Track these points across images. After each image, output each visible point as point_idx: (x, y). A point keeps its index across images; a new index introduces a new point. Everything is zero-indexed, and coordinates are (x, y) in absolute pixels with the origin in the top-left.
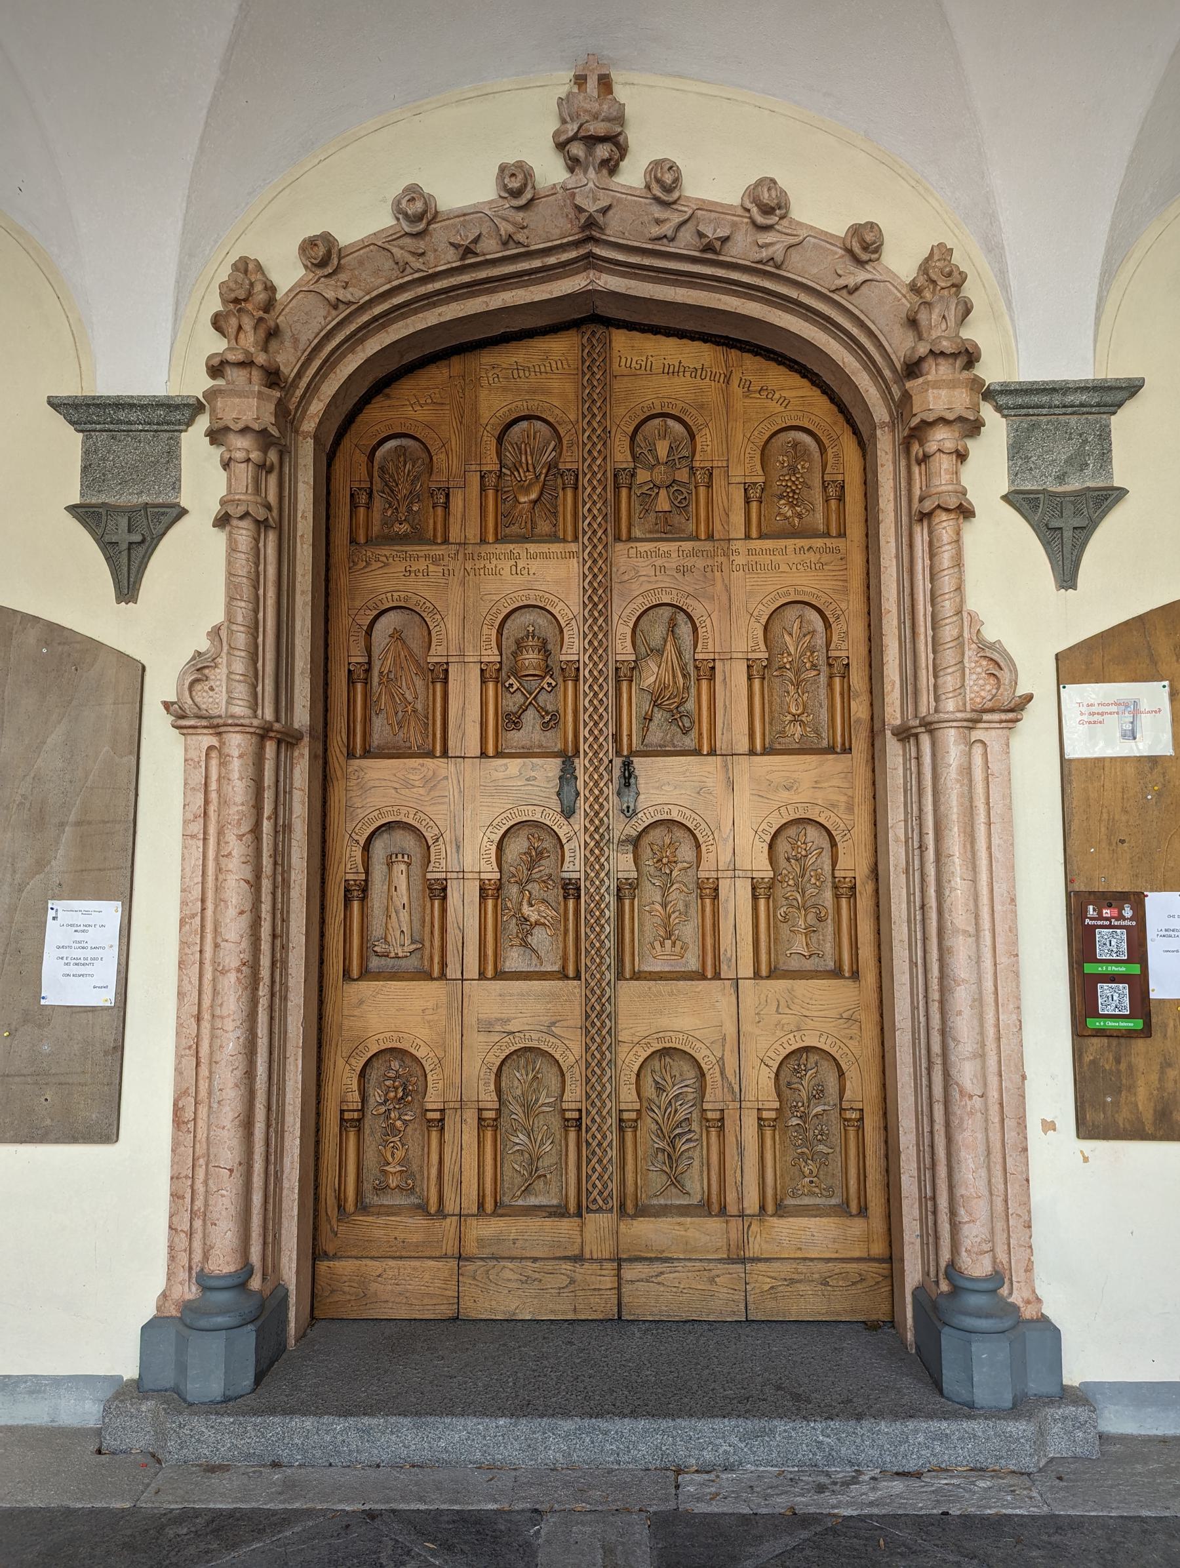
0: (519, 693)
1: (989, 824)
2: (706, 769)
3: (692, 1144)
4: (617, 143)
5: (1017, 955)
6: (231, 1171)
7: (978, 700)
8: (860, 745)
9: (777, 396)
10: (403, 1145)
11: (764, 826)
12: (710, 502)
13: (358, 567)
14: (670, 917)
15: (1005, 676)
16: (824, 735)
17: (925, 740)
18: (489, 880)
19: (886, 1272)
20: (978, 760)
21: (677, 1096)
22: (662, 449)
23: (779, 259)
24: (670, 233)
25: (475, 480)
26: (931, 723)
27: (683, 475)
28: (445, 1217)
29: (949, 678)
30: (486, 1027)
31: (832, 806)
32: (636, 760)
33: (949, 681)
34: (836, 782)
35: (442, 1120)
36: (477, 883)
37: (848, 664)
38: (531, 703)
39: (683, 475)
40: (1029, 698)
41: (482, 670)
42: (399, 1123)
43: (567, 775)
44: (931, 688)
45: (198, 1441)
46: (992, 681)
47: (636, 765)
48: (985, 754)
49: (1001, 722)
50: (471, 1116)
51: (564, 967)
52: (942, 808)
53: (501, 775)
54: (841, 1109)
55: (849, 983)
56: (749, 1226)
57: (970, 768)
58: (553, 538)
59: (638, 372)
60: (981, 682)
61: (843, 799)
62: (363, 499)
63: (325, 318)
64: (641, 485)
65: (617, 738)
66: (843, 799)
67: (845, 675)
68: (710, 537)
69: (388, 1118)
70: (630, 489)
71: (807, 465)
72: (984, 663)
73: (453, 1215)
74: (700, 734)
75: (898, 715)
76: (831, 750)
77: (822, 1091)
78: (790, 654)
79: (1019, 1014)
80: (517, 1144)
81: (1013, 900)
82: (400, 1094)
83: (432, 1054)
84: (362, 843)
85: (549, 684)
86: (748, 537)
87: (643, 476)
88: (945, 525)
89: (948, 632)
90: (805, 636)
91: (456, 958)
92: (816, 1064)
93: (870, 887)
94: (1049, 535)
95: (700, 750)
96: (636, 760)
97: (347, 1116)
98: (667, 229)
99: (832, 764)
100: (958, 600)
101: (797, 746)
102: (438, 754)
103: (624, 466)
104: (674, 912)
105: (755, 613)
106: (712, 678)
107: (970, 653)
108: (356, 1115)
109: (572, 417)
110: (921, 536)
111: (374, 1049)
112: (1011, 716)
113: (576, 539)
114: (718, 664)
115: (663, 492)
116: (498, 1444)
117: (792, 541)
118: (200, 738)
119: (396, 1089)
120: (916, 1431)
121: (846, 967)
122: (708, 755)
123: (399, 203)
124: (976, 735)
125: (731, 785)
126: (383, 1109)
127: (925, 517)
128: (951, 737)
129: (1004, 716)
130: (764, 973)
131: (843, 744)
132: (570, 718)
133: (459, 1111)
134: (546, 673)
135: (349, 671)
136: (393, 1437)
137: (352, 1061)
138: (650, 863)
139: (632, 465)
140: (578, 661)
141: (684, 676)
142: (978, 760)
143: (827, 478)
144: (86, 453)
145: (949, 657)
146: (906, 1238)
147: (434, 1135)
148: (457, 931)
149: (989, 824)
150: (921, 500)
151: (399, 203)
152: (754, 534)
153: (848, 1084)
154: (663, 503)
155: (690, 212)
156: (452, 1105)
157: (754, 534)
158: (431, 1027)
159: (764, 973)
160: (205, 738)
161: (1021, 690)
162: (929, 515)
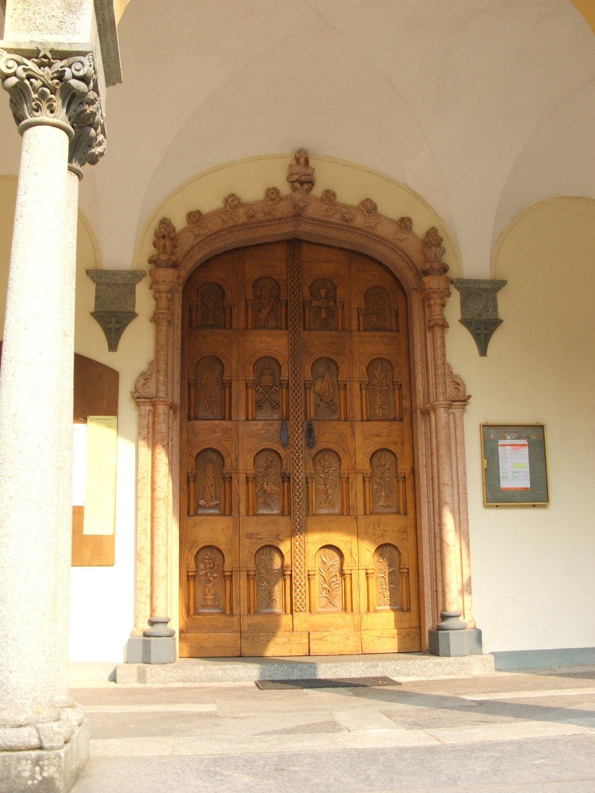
0: (262, 393)
1: (456, 444)
2: (344, 427)
3: (338, 586)
4: (311, 183)
5: (467, 494)
6: (163, 578)
7: (452, 397)
8: (406, 418)
9: (370, 273)
10: (213, 587)
11: (367, 451)
12: (343, 316)
13: (198, 339)
14: (328, 490)
15: (461, 388)
16: (392, 414)
17: (433, 416)
18: (250, 474)
19: (418, 632)
20: (452, 419)
21: (331, 566)
22: (323, 292)
23: (373, 227)
24: (331, 215)
25: (243, 302)
26: (434, 406)
27: (331, 304)
28: (233, 616)
29: (441, 388)
30: (250, 536)
31: (396, 443)
32: (313, 422)
33: (440, 389)
34: (397, 433)
35: (231, 576)
36: (245, 475)
37: (401, 385)
38: (267, 398)
39: (331, 304)
40: (470, 397)
41: (246, 384)
42: (211, 578)
43: (283, 429)
44: (434, 392)
45: (159, 675)
46: (456, 390)
47: (313, 425)
48: (454, 418)
49: (460, 405)
50: (244, 575)
51: (283, 512)
52: (439, 438)
53: (255, 428)
54: (400, 568)
55: (403, 517)
56: (363, 617)
57: (449, 423)
58: (278, 328)
59: (312, 261)
60: (453, 390)
61: (400, 440)
62: (195, 309)
63: (193, 240)
64: (313, 308)
65: (305, 413)
66: (400, 440)
67: (400, 389)
68: (344, 329)
69: (207, 576)
70: (309, 309)
71: (383, 301)
72: (454, 383)
73: (237, 615)
74: (340, 412)
75: (422, 404)
76: (395, 420)
77: (392, 563)
78: (377, 379)
79: (468, 516)
80: (263, 586)
81: (465, 473)
82: (212, 566)
83: (226, 548)
84: (195, 457)
85: (275, 390)
86: (359, 330)
87: (315, 303)
88: (438, 332)
89: (440, 371)
90: (383, 372)
91: (236, 508)
92: (390, 551)
93: (411, 477)
94: (477, 336)
95: (225, 513)
96: (313, 422)
97: (190, 574)
98: (330, 213)
99: (395, 426)
100: (443, 359)
101: (380, 418)
102: (227, 419)
103: (308, 299)
104: (329, 488)
105: (363, 362)
106: (345, 389)
107: (448, 380)
108: (194, 574)
109: (285, 278)
110: (429, 335)
111: (201, 546)
112: (463, 403)
113: (287, 329)
114: (348, 384)
115: (323, 311)
116: (275, 674)
117: (378, 333)
118: (145, 406)
119: (210, 564)
120: (430, 663)
121: (402, 510)
122: (344, 421)
123: (227, 200)
124: (452, 410)
125: (353, 433)
126: (204, 572)
127: (431, 328)
128: (442, 412)
129: (461, 403)
130: (368, 513)
131: (400, 418)
132: (284, 405)
133: (238, 572)
134: (274, 385)
135: (189, 383)
136: (235, 672)
137: (192, 550)
138: (319, 467)
139: (310, 299)
140: (288, 380)
141: (333, 387)
142: (452, 419)
143: (391, 307)
144: (97, 291)
145: (440, 380)
146: (426, 610)
147: (228, 582)
148: (236, 496)
149: (456, 444)
150: (429, 321)
151: (227, 200)
152: (362, 329)
153: (403, 558)
154: (323, 315)
155: (339, 208)
156: (235, 569)
157: (362, 329)
158: (226, 536)
159: (368, 513)
160: (148, 407)
161: (467, 394)
162: (433, 326)
